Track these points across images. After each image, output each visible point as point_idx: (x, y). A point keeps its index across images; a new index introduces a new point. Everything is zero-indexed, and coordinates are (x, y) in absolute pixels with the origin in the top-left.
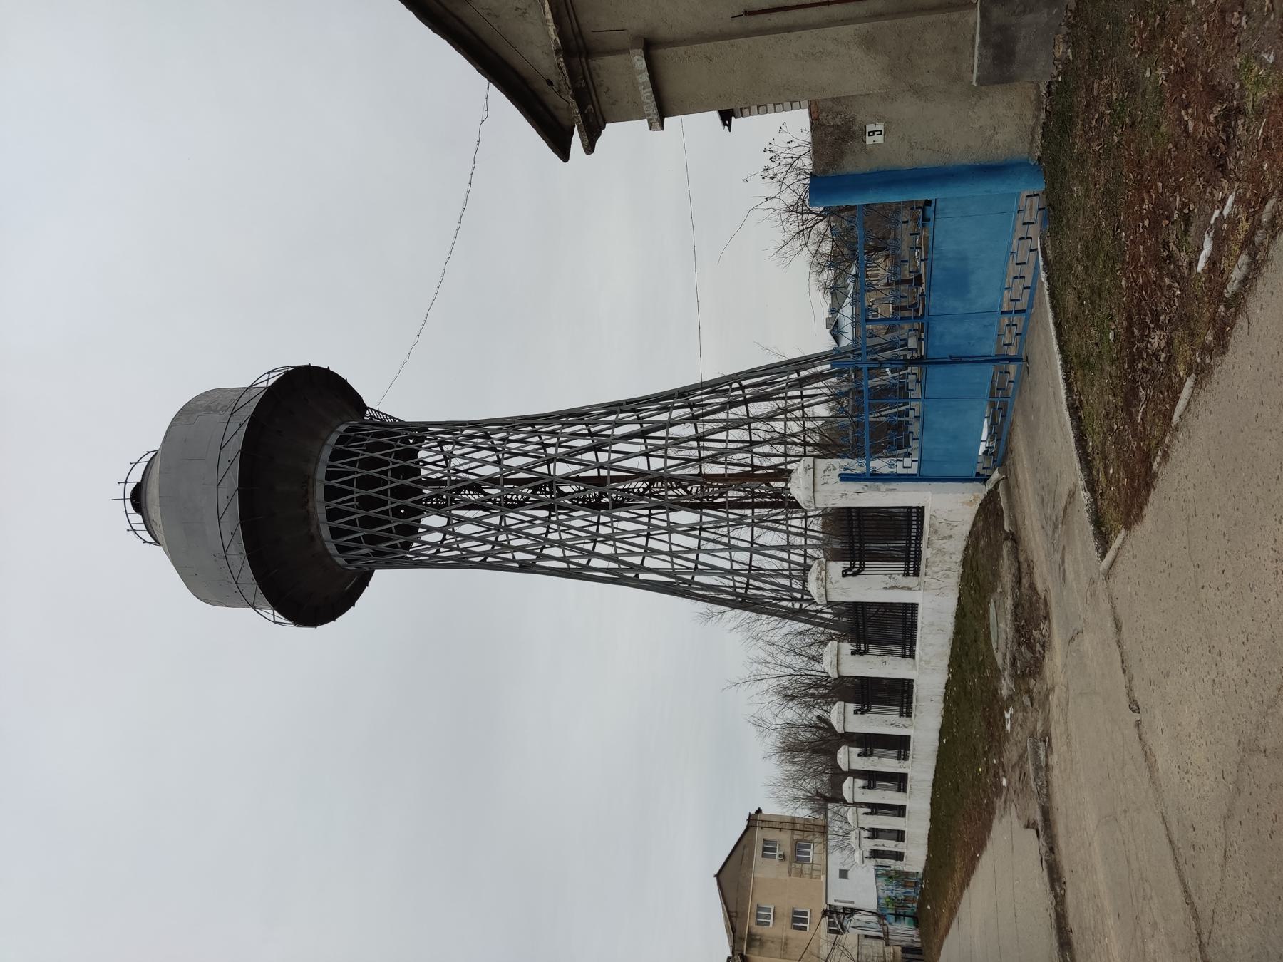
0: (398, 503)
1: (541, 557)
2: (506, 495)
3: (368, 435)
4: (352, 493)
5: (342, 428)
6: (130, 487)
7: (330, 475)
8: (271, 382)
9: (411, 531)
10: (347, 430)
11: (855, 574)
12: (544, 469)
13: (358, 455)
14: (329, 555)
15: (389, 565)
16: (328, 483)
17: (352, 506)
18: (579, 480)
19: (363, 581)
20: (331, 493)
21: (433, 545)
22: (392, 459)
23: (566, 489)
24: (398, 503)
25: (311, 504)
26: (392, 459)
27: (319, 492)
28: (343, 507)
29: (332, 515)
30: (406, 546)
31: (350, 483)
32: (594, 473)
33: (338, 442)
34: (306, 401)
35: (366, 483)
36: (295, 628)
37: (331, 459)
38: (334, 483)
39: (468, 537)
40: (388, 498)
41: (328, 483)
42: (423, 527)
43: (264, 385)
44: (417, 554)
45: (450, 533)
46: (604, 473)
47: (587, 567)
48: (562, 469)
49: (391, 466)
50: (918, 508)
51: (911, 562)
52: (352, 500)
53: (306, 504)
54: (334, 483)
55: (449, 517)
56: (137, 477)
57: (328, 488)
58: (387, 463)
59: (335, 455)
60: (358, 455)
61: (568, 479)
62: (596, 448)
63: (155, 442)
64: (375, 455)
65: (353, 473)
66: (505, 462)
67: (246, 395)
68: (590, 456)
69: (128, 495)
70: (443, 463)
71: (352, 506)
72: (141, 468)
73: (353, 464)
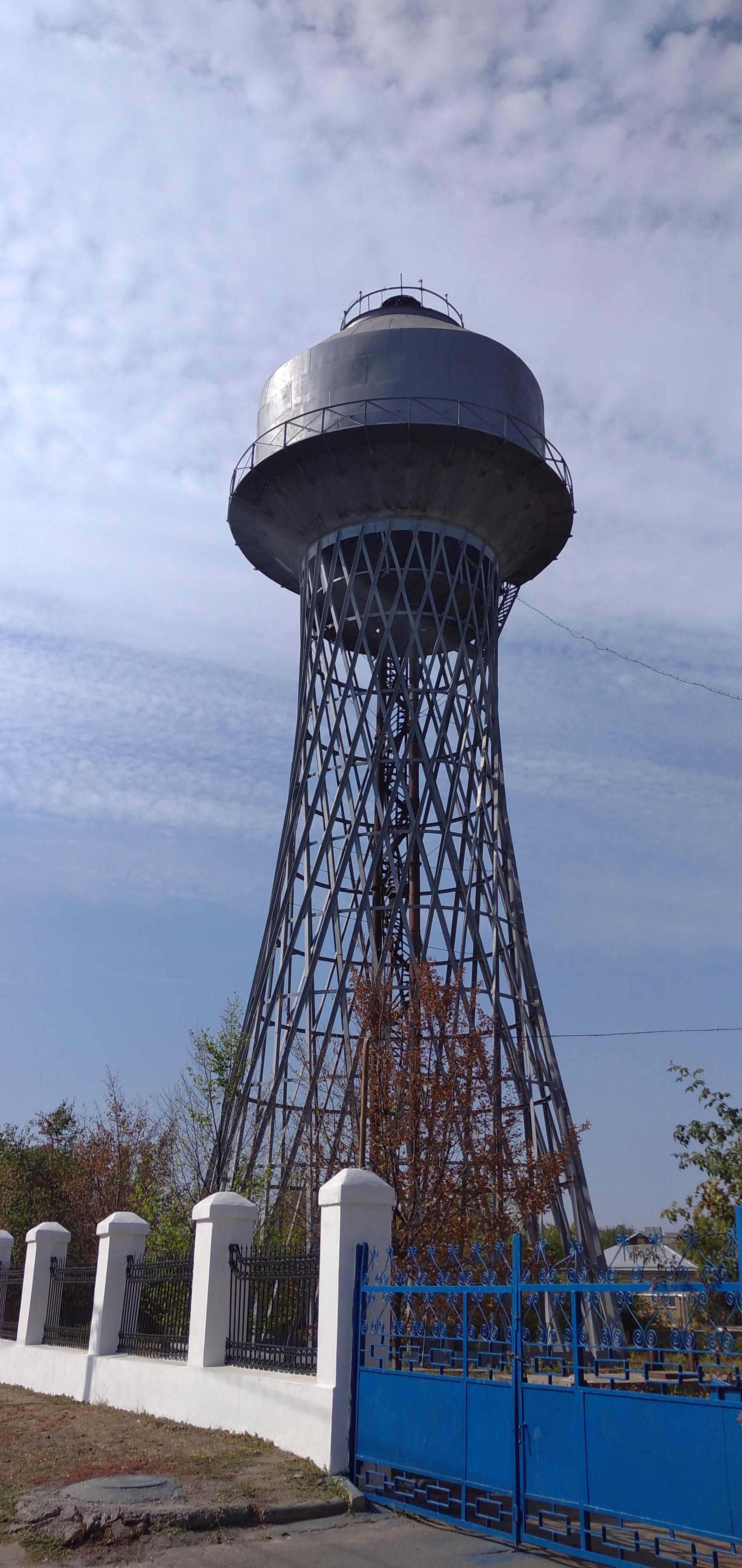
0: (387, 625)
1: (311, 812)
2: (397, 766)
3: (480, 585)
4: (402, 565)
5: (489, 553)
6: (416, 295)
7: (425, 538)
8: (551, 464)
9: (349, 640)
10: (486, 559)
11: (232, 1263)
12: (433, 818)
13: (453, 572)
14: (321, 536)
15: (306, 614)
16: (415, 535)
17: (384, 566)
18: (416, 865)
19: (289, 582)
20: (402, 539)
21: (332, 668)
22: (467, 625)
23: (403, 848)
24: (387, 625)
25: (389, 512)
26: (467, 625)
27: (403, 524)
28: (383, 554)
29: (373, 541)
30: (330, 635)
31: (415, 562)
32: (425, 886)
33: (470, 548)
34: (538, 516)
35: (415, 585)
36: (227, 494)
37: (447, 539)
38: (416, 542)
39: (341, 713)
40: (394, 611)
41: (415, 535)
42: (356, 657)
43: (548, 455)
44: (320, 648)
45: (346, 692)
46: (425, 900)
47: (294, 874)
48: (431, 842)
49: (459, 622)
50: (185, 1352)
51: (234, 1352)
52: (392, 565)
53: (388, 507)
54: (416, 542)
55: (370, 692)
56: (429, 302)
57: (409, 534)
58: (440, 610)
59: (452, 544)
60: (453, 572)
61: (416, 849)
62: (460, 891)
63: (472, 325)
64: (452, 595)
65: (428, 566)
66: (442, 766)
67: (534, 433)
68: (448, 880)
69: (406, 293)
70: (442, 684)
71: (384, 566)
72: (442, 308)
73: (440, 567)
